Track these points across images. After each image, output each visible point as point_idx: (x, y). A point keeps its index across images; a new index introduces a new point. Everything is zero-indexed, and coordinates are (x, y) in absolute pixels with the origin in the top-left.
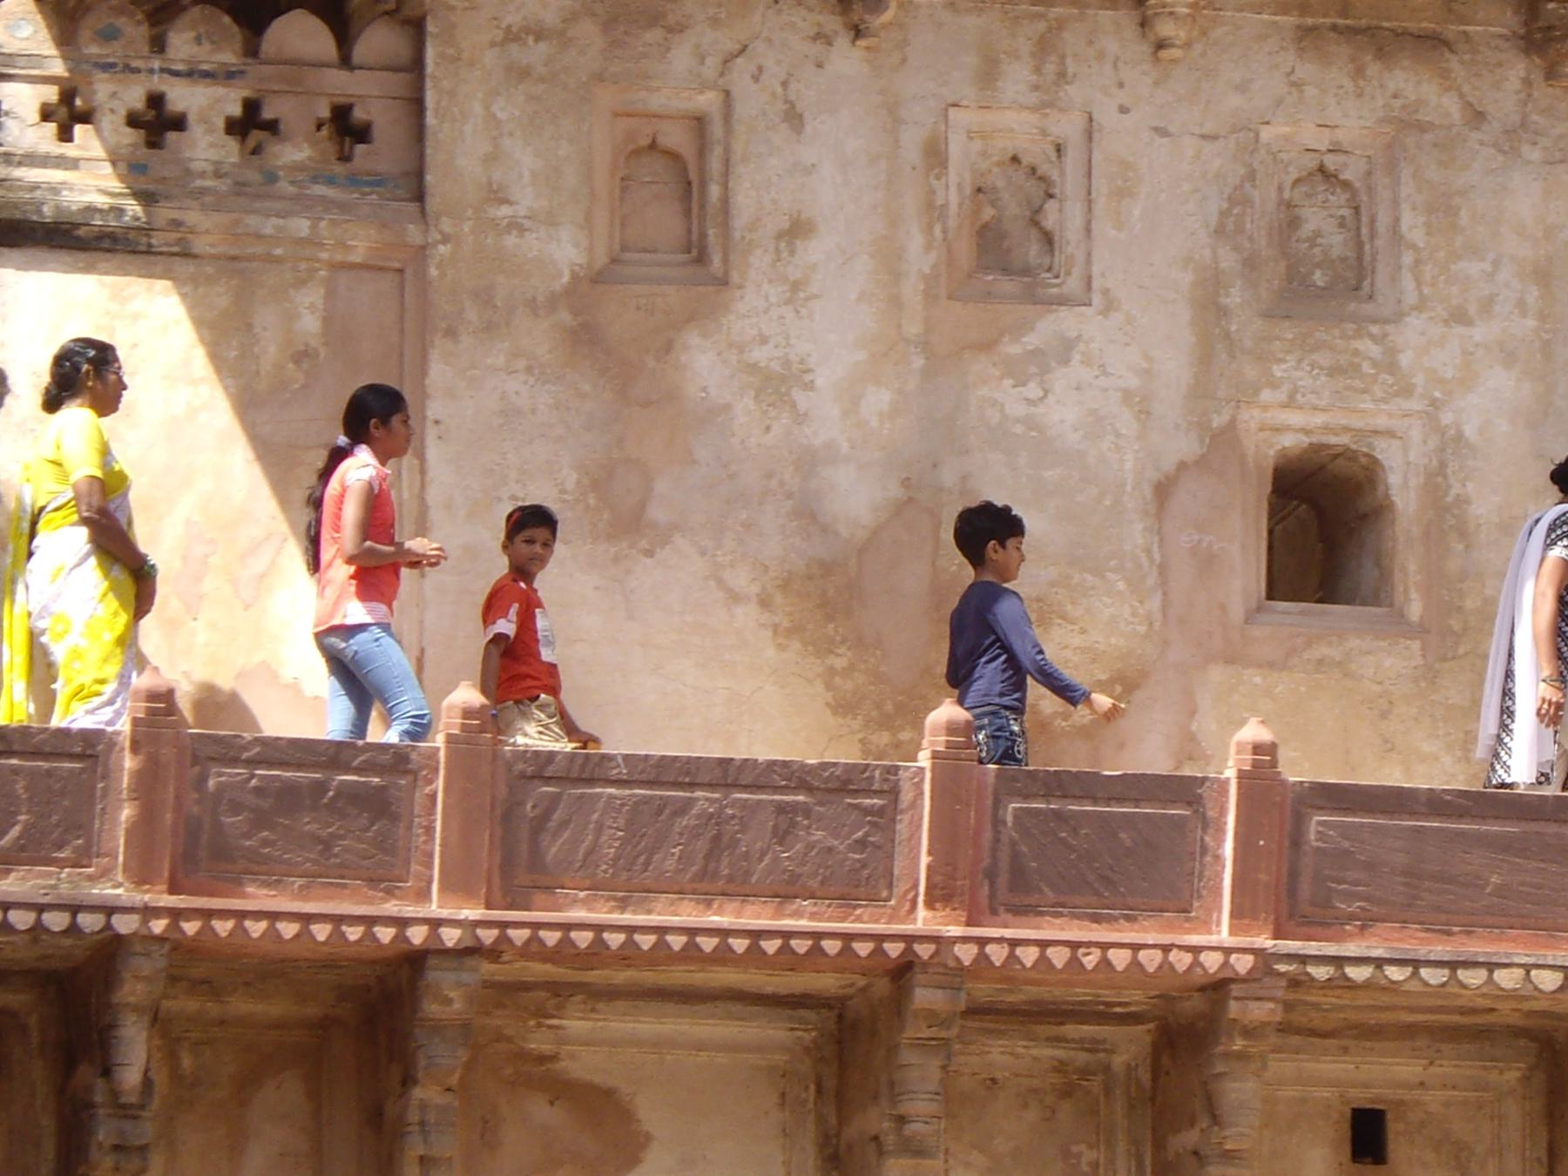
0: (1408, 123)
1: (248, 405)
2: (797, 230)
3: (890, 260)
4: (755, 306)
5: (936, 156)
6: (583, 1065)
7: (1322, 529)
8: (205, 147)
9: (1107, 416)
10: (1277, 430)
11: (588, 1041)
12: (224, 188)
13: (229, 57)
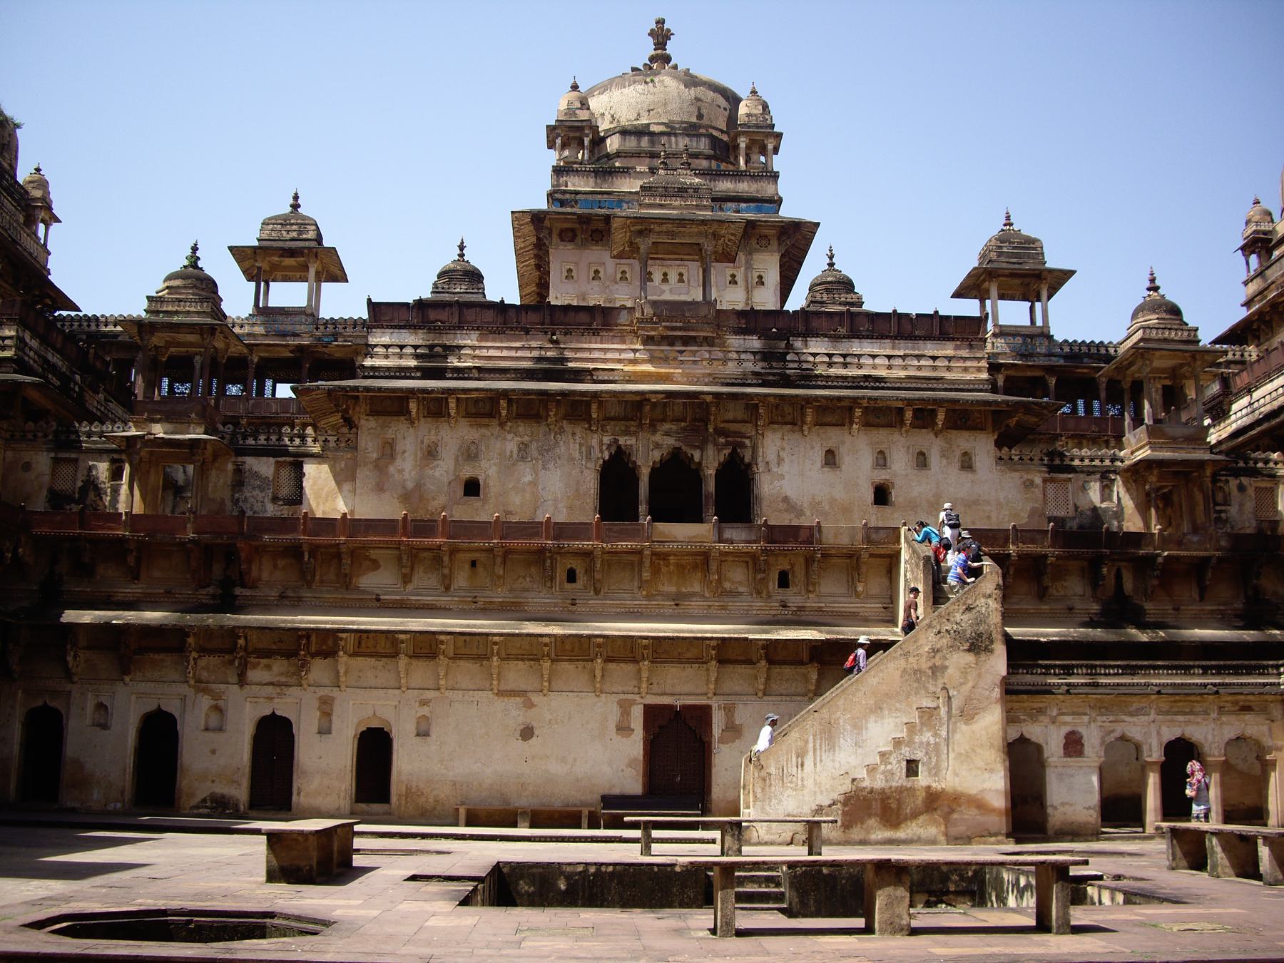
0: (483, 436)
1: (334, 476)
2: (404, 452)
3: (416, 456)
4: (398, 462)
5: (422, 442)
6: (373, 557)
7: (472, 488)
8: (332, 444)
9: (444, 471)
10: (1148, 897)
11: (373, 554)
12: (1241, 606)
13: (843, 590)
